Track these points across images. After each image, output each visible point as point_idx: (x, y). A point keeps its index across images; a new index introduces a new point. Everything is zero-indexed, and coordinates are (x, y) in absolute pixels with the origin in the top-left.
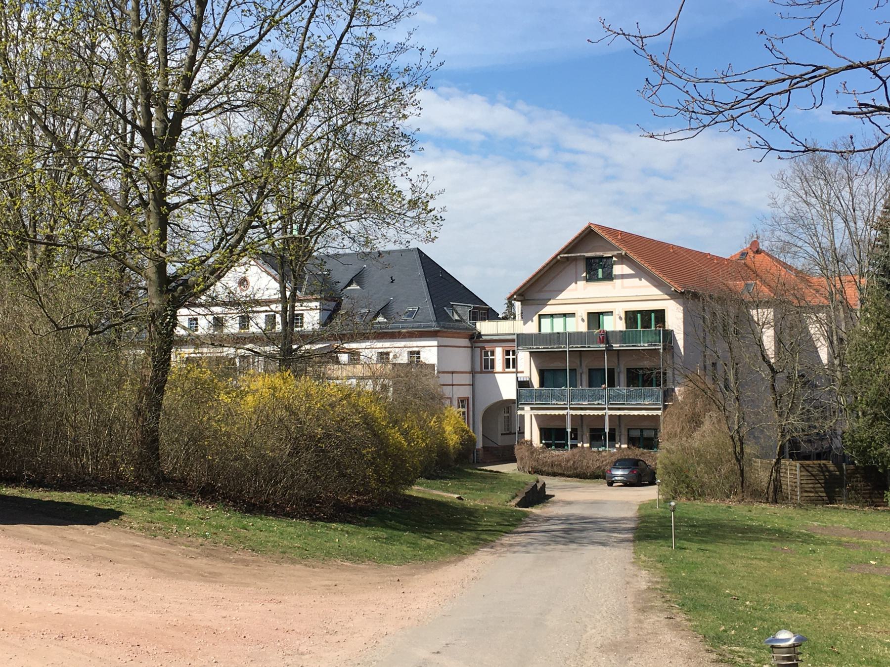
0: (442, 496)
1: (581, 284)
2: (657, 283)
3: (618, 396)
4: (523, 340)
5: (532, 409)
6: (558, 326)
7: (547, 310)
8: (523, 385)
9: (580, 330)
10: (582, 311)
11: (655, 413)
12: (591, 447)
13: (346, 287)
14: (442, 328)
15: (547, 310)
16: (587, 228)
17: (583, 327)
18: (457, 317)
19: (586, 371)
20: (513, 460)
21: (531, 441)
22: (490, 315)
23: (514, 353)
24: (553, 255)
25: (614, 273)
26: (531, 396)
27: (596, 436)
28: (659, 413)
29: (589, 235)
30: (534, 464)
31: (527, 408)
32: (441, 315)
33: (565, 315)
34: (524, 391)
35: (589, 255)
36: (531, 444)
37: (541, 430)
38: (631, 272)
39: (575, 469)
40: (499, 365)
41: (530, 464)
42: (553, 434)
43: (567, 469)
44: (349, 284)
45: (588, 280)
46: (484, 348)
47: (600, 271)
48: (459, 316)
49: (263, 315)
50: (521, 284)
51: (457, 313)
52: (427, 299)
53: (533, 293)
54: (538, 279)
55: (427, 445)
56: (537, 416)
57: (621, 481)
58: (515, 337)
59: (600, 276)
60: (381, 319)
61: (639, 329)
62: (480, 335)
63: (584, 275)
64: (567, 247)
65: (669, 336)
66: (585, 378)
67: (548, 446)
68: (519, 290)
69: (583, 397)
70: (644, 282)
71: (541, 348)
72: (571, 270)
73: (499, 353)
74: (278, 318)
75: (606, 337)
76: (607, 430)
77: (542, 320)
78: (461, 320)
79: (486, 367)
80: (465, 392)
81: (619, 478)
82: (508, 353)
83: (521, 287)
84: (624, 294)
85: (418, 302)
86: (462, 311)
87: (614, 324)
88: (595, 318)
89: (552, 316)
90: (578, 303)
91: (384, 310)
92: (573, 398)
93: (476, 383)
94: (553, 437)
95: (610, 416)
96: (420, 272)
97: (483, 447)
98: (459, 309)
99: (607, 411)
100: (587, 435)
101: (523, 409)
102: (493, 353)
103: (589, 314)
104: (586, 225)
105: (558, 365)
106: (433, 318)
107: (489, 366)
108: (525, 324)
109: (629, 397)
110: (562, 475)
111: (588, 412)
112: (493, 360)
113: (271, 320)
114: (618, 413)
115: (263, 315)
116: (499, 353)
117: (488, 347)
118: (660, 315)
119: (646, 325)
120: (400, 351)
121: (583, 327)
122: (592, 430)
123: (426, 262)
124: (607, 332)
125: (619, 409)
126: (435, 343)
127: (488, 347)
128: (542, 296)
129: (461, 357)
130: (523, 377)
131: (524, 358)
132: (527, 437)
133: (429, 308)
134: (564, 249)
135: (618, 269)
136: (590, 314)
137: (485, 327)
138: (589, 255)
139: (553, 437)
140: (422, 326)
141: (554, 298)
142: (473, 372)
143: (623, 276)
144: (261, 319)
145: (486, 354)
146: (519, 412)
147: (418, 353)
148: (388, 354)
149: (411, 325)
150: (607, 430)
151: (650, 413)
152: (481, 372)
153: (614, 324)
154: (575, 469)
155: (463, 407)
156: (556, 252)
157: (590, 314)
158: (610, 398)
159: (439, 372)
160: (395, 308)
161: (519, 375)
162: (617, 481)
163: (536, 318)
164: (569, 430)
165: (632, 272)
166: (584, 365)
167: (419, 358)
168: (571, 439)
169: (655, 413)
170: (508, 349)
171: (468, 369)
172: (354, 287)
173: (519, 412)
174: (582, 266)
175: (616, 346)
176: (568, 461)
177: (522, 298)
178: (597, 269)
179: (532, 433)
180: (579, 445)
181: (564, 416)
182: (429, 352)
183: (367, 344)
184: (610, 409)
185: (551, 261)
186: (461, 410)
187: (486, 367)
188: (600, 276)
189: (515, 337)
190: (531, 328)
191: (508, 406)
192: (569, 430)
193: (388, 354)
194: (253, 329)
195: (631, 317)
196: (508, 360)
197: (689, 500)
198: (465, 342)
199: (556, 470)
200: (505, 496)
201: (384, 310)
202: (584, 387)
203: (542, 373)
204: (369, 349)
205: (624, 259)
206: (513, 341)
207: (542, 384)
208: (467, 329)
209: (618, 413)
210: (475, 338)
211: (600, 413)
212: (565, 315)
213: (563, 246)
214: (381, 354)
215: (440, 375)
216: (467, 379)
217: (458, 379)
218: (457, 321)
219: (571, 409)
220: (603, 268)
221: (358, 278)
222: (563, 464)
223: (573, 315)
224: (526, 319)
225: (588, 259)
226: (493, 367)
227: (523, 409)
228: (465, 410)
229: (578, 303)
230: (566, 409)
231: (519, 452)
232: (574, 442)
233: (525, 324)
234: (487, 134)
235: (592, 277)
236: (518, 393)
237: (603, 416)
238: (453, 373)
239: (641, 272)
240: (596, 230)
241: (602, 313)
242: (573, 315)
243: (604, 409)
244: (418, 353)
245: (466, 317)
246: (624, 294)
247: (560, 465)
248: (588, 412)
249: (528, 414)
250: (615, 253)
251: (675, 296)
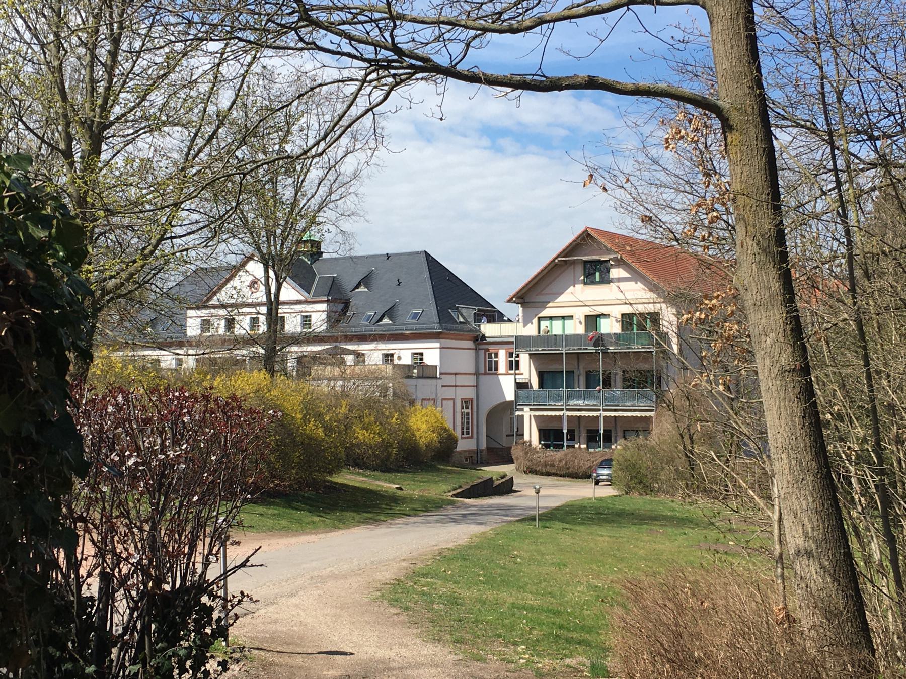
0: (382, 487)
1: (579, 287)
2: (653, 288)
3: (613, 399)
4: (521, 342)
5: (531, 410)
6: (557, 328)
7: (546, 313)
8: (521, 386)
9: (578, 333)
10: (580, 314)
11: (648, 414)
12: (588, 447)
13: (354, 289)
14: (445, 329)
15: (546, 313)
16: (584, 232)
17: (581, 330)
18: (461, 320)
19: (583, 372)
20: (510, 461)
21: (530, 442)
22: (495, 316)
23: (518, 356)
24: (551, 258)
25: (611, 276)
26: (528, 398)
27: (592, 437)
28: (652, 414)
29: (586, 239)
30: (529, 463)
31: (526, 409)
32: (444, 316)
33: (563, 318)
34: (523, 392)
35: (585, 258)
36: (530, 445)
37: (540, 430)
38: (627, 275)
39: (568, 469)
40: (502, 367)
41: (525, 463)
42: (551, 435)
43: (560, 468)
44: (357, 287)
45: (585, 284)
46: (488, 350)
47: (598, 274)
48: (464, 318)
49: (248, 317)
50: (517, 289)
51: (462, 315)
52: (432, 301)
53: (530, 296)
54: (536, 283)
55: (383, 439)
56: (534, 416)
57: (607, 480)
58: (513, 340)
59: (598, 279)
60: (386, 321)
61: (635, 331)
62: (484, 337)
63: (582, 278)
64: (564, 250)
65: (664, 337)
66: (583, 380)
67: (547, 446)
68: (518, 293)
69: (579, 397)
70: (640, 285)
71: (540, 350)
72: (569, 273)
73: (502, 354)
74: (262, 319)
75: (600, 340)
76: (602, 432)
77: (542, 323)
78: (466, 322)
79: (490, 369)
80: (470, 393)
81: (605, 478)
82: (511, 355)
83: (520, 290)
84: (618, 298)
85: (422, 305)
86: (468, 312)
87: (610, 327)
88: (592, 321)
89: (551, 318)
90: (575, 307)
91: (390, 313)
92: (569, 398)
93: (480, 383)
94: (552, 437)
95: (605, 417)
96: (426, 274)
97: (488, 448)
98: (464, 311)
99: (601, 412)
100: (584, 435)
101: (522, 410)
102: (496, 355)
103: (586, 316)
104: (583, 229)
105: (559, 367)
106: (436, 319)
107: (492, 368)
108: (525, 326)
109: (623, 398)
110: (556, 475)
111: (583, 414)
112: (496, 362)
113: (254, 322)
114: (613, 414)
115: (248, 317)
116: (502, 354)
117: (492, 349)
118: (655, 318)
119: (642, 328)
120: (404, 353)
121: (581, 330)
122: (589, 431)
123: (433, 265)
124: (602, 334)
125: (615, 410)
126: (438, 345)
127: (492, 349)
128: (541, 298)
129: (464, 358)
130: (520, 379)
131: (524, 358)
132: (526, 437)
133: (434, 311)
134: (561, 253)
135: (615, 273)
136: (587, 317)
137: (489, 330)
138: (585, 258)
139: (552, 437)
140: (424, 329)
141: (553, 301)
142: (477, 374)
143: (619, 280)
144: (246, 322)
145: (490, 356)
146: (517, 413)
147: (422, 354)
148: (392, 355)
149: (415, 327)
150: (602, 432)
151: (644, 414)
152: (485, 374)
153: (610, 327)
154: (568, 469)
155: (467, 408)
156: (554, 256)
157: (587, 317)
158: (605, 399)
159: (441, 374)
160: (400, 310)
161: (517, 377)
162: (603, 481)
163: (535, 321)
164: (565, 431)
165: (628, 275)
166: (581, 367)
167: (421, 359)
168: (567, 439)
169: (648, 414)
170: (511, 351)
171: (473, 371)
172: (362, 289)
173: (517, 413)
174: (580, 269)
175: (612, 349)
176: (560, 461)
177: (521, 301)
178: (595, 272)
179: (531, 434)
180: (577, 446)
181: (560, 417)
182: (432, 354)
183: (372, 346)
184: (604, 410)
185: (549, 264)
186: (465, 411)
187: (490, 369)
188: (598, 279)
189: (513, 340)
190: (531, 330)
191: (509, 407)
192: (565, 431)
193: (392, 355)
194: (238, 331)
195: (627, 320)
196: (511, 362)
197: (641, 495)
198: (470, 344)
199: (549, 469)
200: (445, 487)
201: (390, 313)
202: (617, 391)
203: (541, 375)
204: (374, 353)
205: (620, 263)
206: (512, 343)
207: (541, 385)
208: (471, 331)
209: (613, 414)
210: (479, 340)
211: (561, 413)
212: (563, 318)
213: (560, 250)
214: (386, 355)
215: (443, 376)
216: (471, 380)
217: (461, 380)
218: (461, 323)
219: (567, 410)
220: (600, 270)
221: (366, 281)
222: (556, 464)
223: (571, 317)
224: (527, 321)
225: (586, 262)
226: (496, 369)
227: (522, 410)
228: (469, 411)
229: (575, 307)
230: (562, 410)
231: (516, 452)
232: (571, 443)
233: (525, 326)
234: (569, 128)
235: (589, 279)
236: (517, 395)
237: (598, 417)
238: (456, 374)
239: (637, 276)
240: (592, 234)
241: (599, 316)
242: (571, 317)
243: (599, 410)
244: (422, 354)
245: (471, 320)
246: (618, 298)
247: (553, 465)
248: (583, 414)
249: (527, 413)
250: (611, 257)
251: (672, 299)
